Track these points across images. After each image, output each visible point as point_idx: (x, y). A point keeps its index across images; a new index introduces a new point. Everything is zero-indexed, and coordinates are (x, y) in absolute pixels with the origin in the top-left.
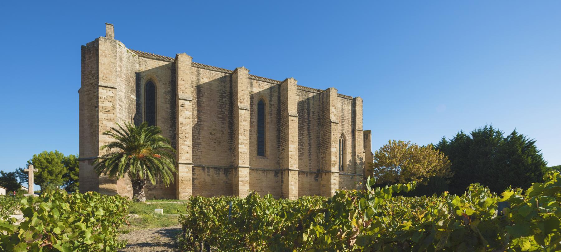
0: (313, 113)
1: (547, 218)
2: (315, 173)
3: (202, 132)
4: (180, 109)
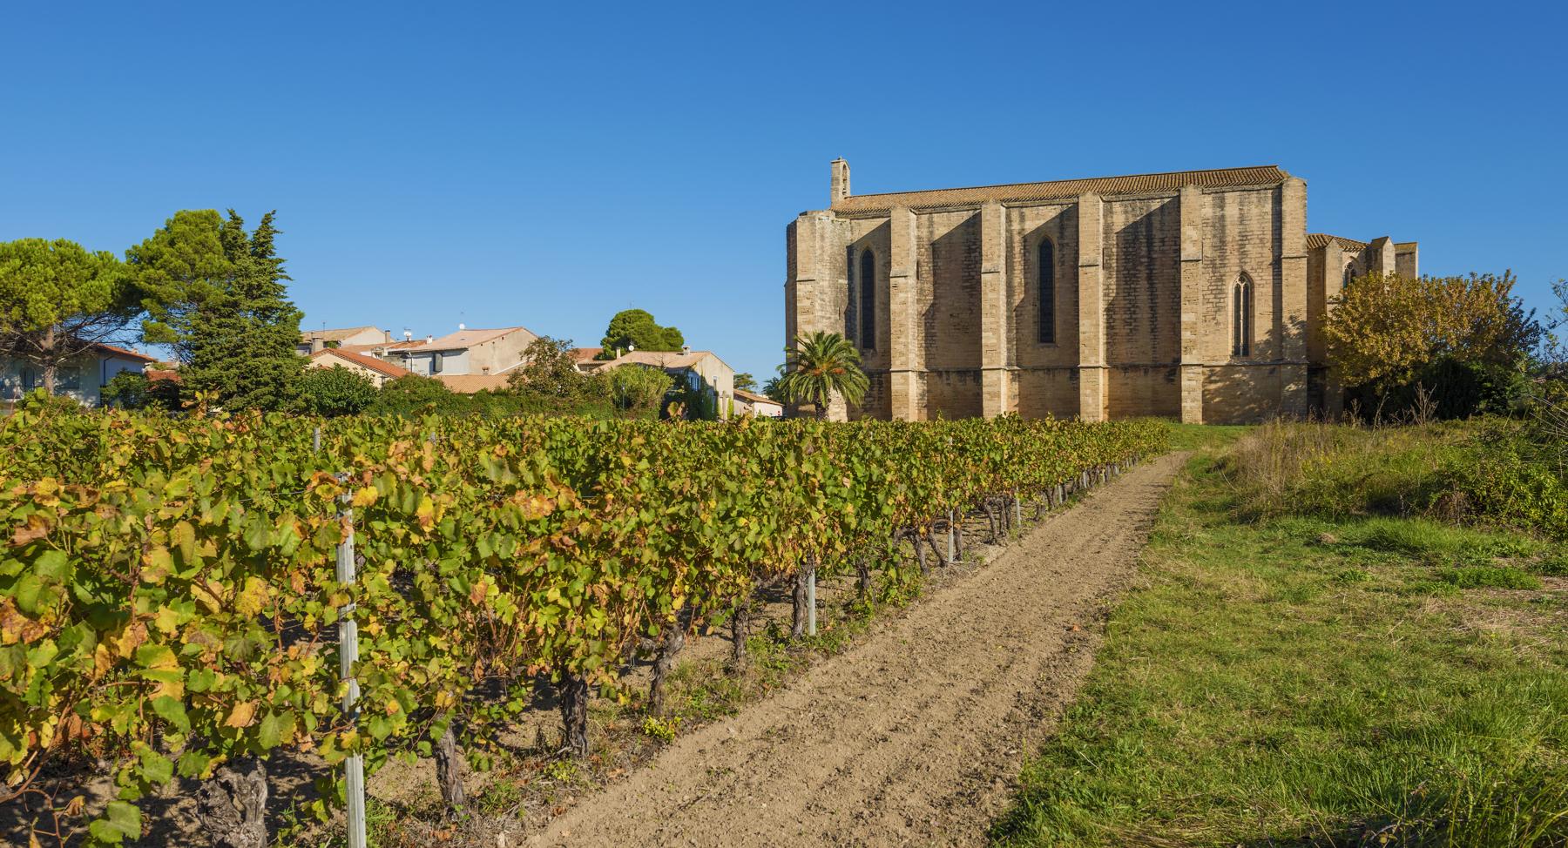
0: (1162, 241)
1: (324, 371)
2: (1165, 366)
3: (938, 315)
4: (892, 291)
